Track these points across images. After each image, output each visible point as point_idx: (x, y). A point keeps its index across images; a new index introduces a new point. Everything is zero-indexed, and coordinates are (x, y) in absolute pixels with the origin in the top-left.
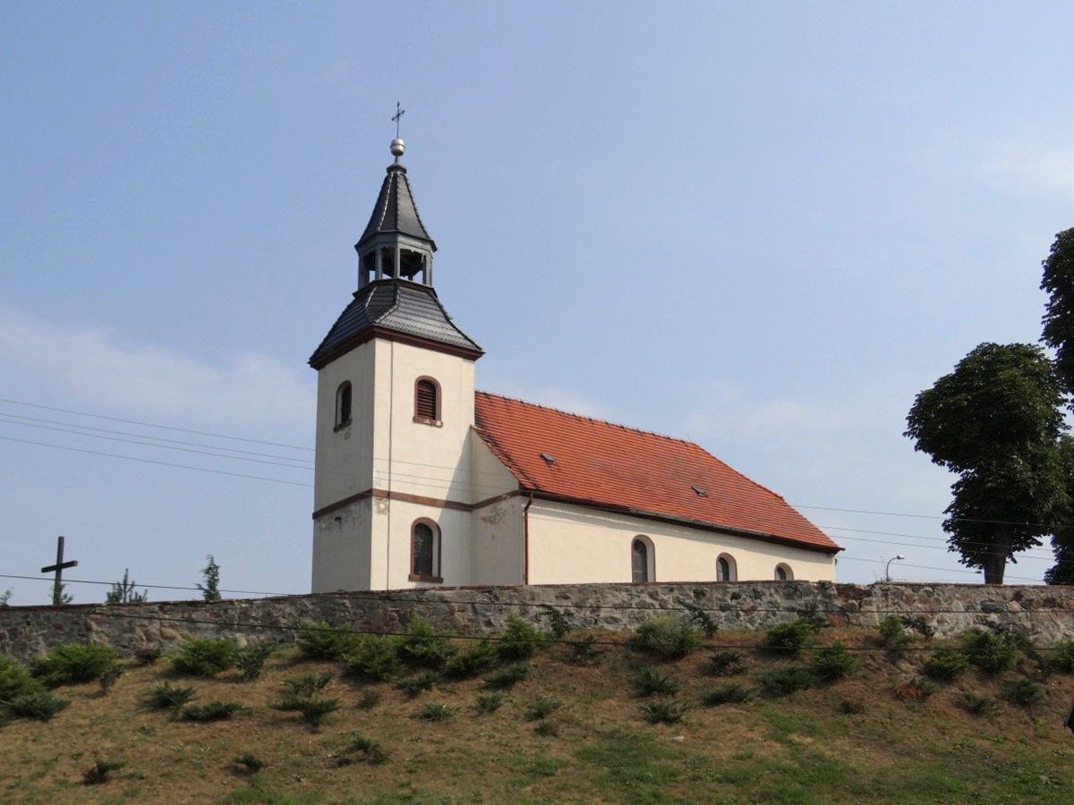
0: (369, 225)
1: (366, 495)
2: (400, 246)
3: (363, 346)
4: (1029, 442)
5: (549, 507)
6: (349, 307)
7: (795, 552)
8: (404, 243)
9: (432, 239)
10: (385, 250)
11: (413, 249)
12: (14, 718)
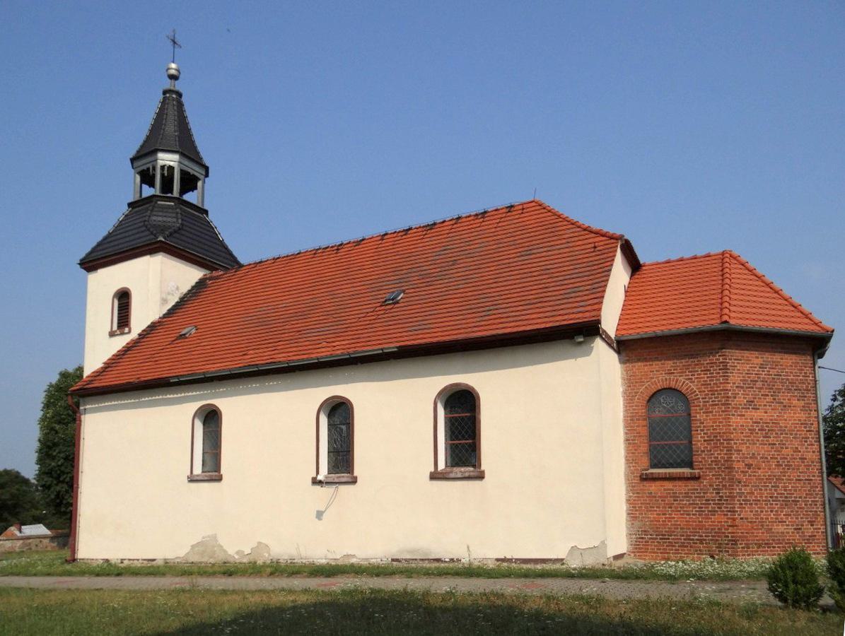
2: (160, 163)
11: (192, 172)
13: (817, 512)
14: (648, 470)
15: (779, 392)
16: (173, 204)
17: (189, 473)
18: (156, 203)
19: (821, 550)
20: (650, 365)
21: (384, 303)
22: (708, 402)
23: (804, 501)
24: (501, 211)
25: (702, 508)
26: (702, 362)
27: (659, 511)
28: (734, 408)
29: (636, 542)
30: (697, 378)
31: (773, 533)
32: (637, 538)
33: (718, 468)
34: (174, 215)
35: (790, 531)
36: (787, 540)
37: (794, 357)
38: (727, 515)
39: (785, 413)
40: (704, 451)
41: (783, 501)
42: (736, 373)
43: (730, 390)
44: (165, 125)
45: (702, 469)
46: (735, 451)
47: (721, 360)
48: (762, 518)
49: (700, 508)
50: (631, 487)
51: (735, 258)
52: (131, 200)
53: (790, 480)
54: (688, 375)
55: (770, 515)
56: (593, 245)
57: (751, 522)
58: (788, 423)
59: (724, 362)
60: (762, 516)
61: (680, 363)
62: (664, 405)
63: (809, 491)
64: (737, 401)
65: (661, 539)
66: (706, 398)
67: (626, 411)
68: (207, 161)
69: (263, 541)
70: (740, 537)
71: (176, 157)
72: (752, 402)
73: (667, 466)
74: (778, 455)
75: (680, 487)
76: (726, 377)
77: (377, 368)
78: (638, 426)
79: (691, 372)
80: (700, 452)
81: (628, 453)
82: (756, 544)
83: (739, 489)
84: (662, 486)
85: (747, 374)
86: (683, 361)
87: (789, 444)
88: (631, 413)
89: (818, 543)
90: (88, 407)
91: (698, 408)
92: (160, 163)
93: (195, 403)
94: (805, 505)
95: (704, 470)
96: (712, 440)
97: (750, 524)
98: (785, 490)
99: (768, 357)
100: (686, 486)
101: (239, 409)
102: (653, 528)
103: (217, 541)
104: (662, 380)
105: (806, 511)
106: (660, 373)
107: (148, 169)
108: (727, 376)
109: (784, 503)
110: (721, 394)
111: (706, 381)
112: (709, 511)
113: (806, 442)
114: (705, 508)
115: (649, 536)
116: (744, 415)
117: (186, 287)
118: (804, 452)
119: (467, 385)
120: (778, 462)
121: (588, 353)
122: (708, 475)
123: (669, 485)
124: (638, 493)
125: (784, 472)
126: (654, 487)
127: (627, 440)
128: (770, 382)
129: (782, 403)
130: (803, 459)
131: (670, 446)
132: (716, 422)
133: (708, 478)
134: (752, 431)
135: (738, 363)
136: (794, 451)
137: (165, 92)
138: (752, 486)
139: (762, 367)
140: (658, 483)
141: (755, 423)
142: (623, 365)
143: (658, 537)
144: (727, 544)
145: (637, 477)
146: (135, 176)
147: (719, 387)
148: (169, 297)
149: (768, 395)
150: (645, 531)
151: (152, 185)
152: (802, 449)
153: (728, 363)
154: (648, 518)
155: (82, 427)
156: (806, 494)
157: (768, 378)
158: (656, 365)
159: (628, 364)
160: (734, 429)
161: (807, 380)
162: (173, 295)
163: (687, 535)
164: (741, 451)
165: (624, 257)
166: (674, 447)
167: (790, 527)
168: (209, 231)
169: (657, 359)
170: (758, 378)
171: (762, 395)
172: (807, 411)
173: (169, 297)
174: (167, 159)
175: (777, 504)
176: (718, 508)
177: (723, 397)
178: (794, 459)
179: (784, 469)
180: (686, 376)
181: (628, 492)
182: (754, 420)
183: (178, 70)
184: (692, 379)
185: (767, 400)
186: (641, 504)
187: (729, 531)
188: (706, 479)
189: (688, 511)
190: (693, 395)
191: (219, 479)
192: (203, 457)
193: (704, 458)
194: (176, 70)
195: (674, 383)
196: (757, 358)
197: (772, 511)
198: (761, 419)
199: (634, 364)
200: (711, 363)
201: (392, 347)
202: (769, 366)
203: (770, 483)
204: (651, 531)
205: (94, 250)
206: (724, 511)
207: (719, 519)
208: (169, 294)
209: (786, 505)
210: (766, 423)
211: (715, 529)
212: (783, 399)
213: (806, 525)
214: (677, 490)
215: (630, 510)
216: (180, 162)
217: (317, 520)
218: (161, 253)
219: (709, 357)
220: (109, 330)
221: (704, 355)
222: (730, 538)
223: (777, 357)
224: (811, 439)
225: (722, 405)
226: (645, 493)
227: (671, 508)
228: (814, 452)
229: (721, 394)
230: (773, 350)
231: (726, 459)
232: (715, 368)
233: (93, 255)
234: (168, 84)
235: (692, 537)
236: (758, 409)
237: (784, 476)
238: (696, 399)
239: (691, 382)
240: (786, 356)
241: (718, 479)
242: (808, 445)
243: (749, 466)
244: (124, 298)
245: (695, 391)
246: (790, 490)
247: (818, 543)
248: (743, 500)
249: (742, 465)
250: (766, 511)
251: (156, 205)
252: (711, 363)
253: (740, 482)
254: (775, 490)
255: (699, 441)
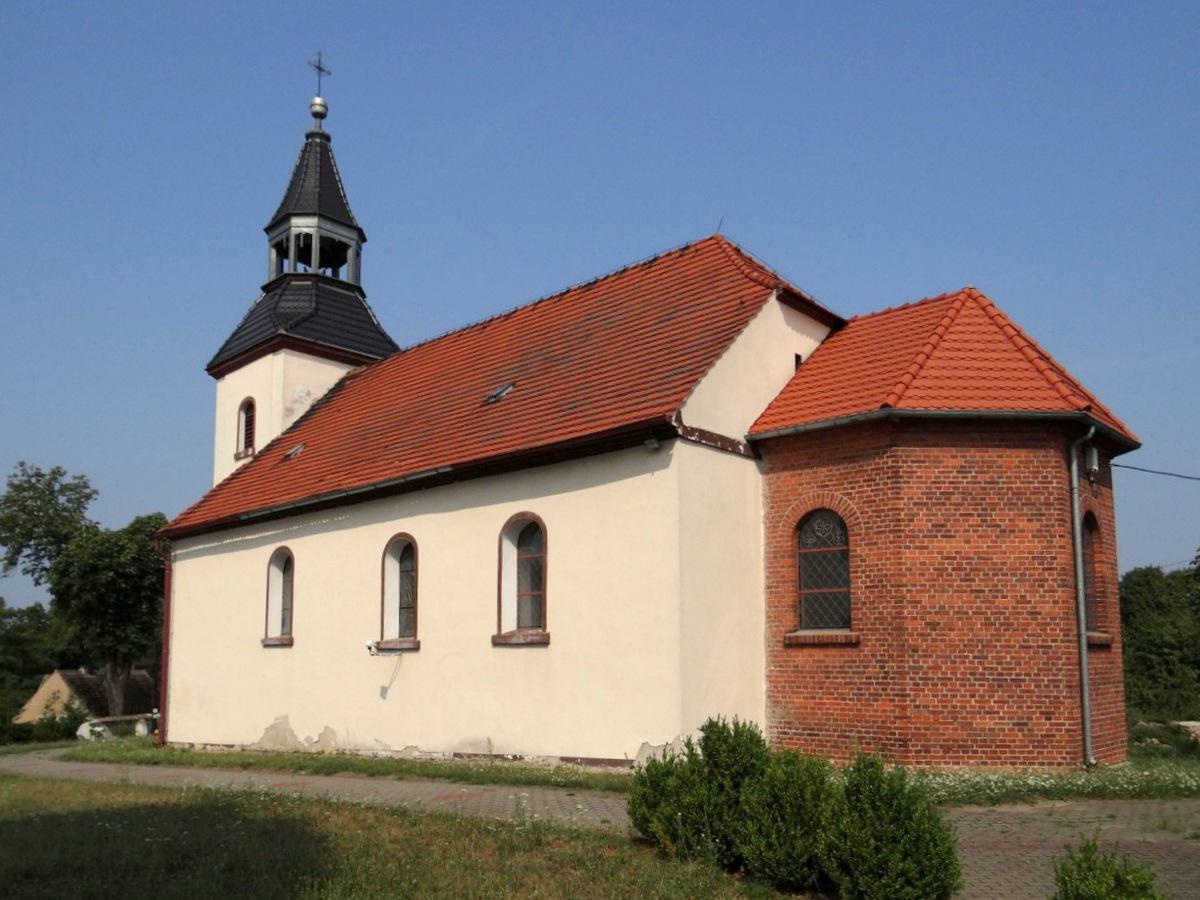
0: (283, 205)
2: (295, 231)
5: (196, 544)
7: (525, 480)
9: (360, 225)
11: (337, 237)
12: (335, 822)
13: (1059, 698)
14: (795, 631)
15: (994, 510)
16: (310, 283)
17: (263, 637)
18: (289, 284)
19: (1064, 758)
20: (799, 475)
21: (486, 403)
22: (871, 528)
23: (1035, 681)
24: (673, 256)
25: (861, 689)
26: (865, 468)
27: (807, 693)
28: (908, 537)
29: (778, 738)
30: (858, 492)
31: (975, 729)
32: (779, 733)
33: (884, 629)
34: (308, 298)
35: (1006, 727)
36: (1001, 741)
37: (1023, 453)
38: (893, 700)
39: (1002, 542)
40: (865, 603)
41: (993, 680)
42: (914, 483)
43: (903, 509)
44: (304, 180)
45: (862, 630)
46: (909, 602)
47: (890, 464)
48: (955, 707)
49: (859, 689)
50: (773, 658)
51: (975, 299)
52: (266, 281)
53: (1009, 647)
54: (846, 489)
55: (969, 702)
56: (739, 301)
57: (933, 712)
58: (1009, 558)
59: (894, 467)
60: (954, 703)
61: (837, 470)
62: (819, 534)
63: (1044, 664)
64: (915, 526)
65: (809, 735)
66: (868, 523)
67: (768, 544)
68: (360, 222)
69: (331, 726)
70: (913, 735)
71: (313, 221)
72: (942, 526)
73: (821, 625)
74: (987, 608)
75: (834, 658)
76: (897, 491)
77: (441, 495)
78: (782, 567)
79: (851, 483)
80: (859, 605)
81: (770, 607)
82: (941, 746)
83: (914, 662)
84: (810, 656)
85: (935, 482)
86: (841, 467)
87: (1008, 591)
88: (775, 547)
89: (1058, 747)
90: (178, 552)
91: (858, 538)
92: (295, 231)
93: (268, 546)
94: (1036, 686)
95: (865, 632)
96: (876, 587)
97: (931, 716)
98: (998, 663)
99: (974, 454)
100: (841, 656)
101: (312, 547)
102: (799, 719)
103: (288, 723)
104: (814, 496)
105: (1037, 697)
106: (814, 486)
107: (282, 240)
108: (898, 488)
109: (996, 683)
110: (888, 516)
111: (870, 496)
112: (870, 694)
113: (1043, 586)
114: (866, 689)
115: (794, 731)
116: (927, 548)
117: (320, 392)
118: (1036, 602)
119: (533, 514)
120: (986, 619)
121: (666, 465)
122: (870, 640)
123: (819, 654)
124: (780, 666)
125: (998, 635)
126: (801, 657)
127: (769, 587)
128: (977, 494)
129: (999, 526)
130: (1034, 614)
131: (825, 596)
132: (881, 560)
133: (870, 643)
134: (941, 571)
135: (920, 467)
136: (1017, 602)
137: (308, 136)
138: (938, 657)
139: (962, 470)
140: (806, 651)
141: (947, 558)
142: (764, 476)
143: (806, 732)
144: (894, 745)
145: (779, 641)
146: (270, 252)
147: (886, 505)
148: (297, 406)
149: (971, 515)
150: (789, 723)
151: (307, 261)
152: (1034, 599)
153: (900, 467)
154: (793, 703)
155: (173, 578)
156: (1039, 669)
157: (974, 489)
158: (806, 475)
159: (771, 475)
160: (907, 569)
161: (1048, 488)
162: (301, 402)
163: (842, 731)
164: (920, 602)
165: (785, 306)
166: (830, 597)
167: (1007, 721)
168: (358, 314)
169: (807, 465)
170: (954, 488)
171: (961, 515)
172: (1045, 537)
173: (297, 406)
174: (303, 225)
175: (983, 685)
176: (883, 689)
177: (892, 521)
178: (1018, 613)
179: (998, 630)
180: (844, 489)
181: (768, 664)
182: (945, 555)
183: (324, 106)
184: (851, 494)
185: (971, 523)
186: (785, 682)
187: (897, 725)
188: (868, 646)
189: (843, 694)
190: (852, 518)
191: (544, 642)
192: (283, 615)
193: (865, 613)
194: (321, 105)
195: (829, 500)
196: (954, 457)
197: (972, 696)
198: (957, 552)
199: (779, 474)
200: (877, 469)
201: (444, 465)
202: (976, 469)
203: (972, 652)
204: (797, 722)
205: (222, 350)
206: (889, 695)
207: (883, 708)
208: (295, 401)
209: (999, 686)
210: (967, 558)
211: (877, 722)
212: (1000, 520)
213: (1037, 718)
214: (829, 661)
215: (773, 691)
216: (319, 227)
217: (380, 698)
218: (284, 350)
219: (874, 459)
220: (235, 452)
221: (868, 457)
222: (897, 736)
223: (991, 454)
224: (1050, 582)
225: (890, 532)
226: (790, 667)
227: (821, 688)
228: (1055, 602)
229: (888, 516)
230: (985, 443)
231: (894, 615)
232: (882, 476)
233: (221, 356)
234: (312, 125)
235: (847, 734)
236: (954, 537)
237: (999, 641)
238: (855, 525)
239: (850, 499)
240: (1008, 452)
241: (884, 645)
242: (1045, 591)
243: (933, 626)
244: (248, 407)
245: (855, 513)
246: (1010, 663)
247: (1058, 747)
248: (921, 679)
249: (920, 625)
250: (962, 696)
251: (289, 287)
252: (877, 469)
253: (916, 651)
254: (980, 663)
255: (859, 588)
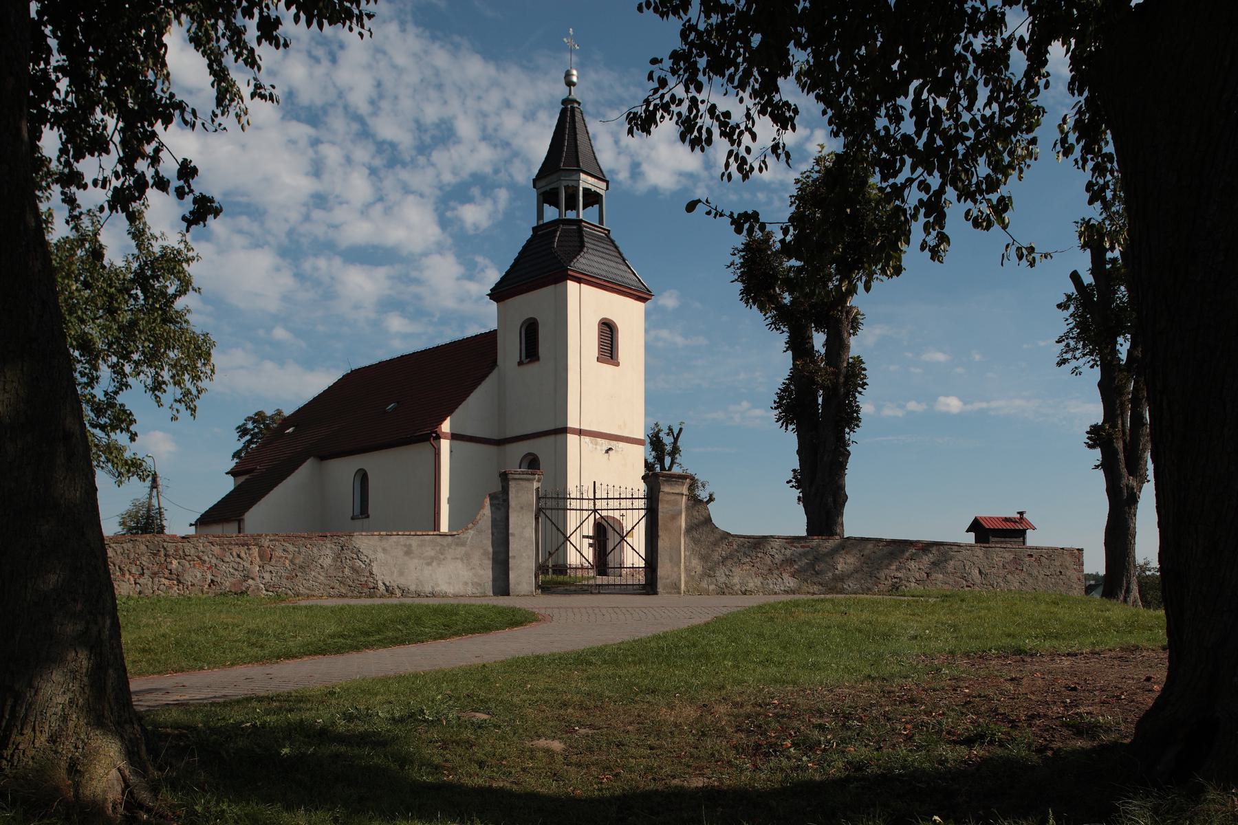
1: (564, 430)
3: (551, 287)
4: (798, 264)
6: (529, 242)
8: (587, 182)
10: (567, 187)
11: (593, 189)
